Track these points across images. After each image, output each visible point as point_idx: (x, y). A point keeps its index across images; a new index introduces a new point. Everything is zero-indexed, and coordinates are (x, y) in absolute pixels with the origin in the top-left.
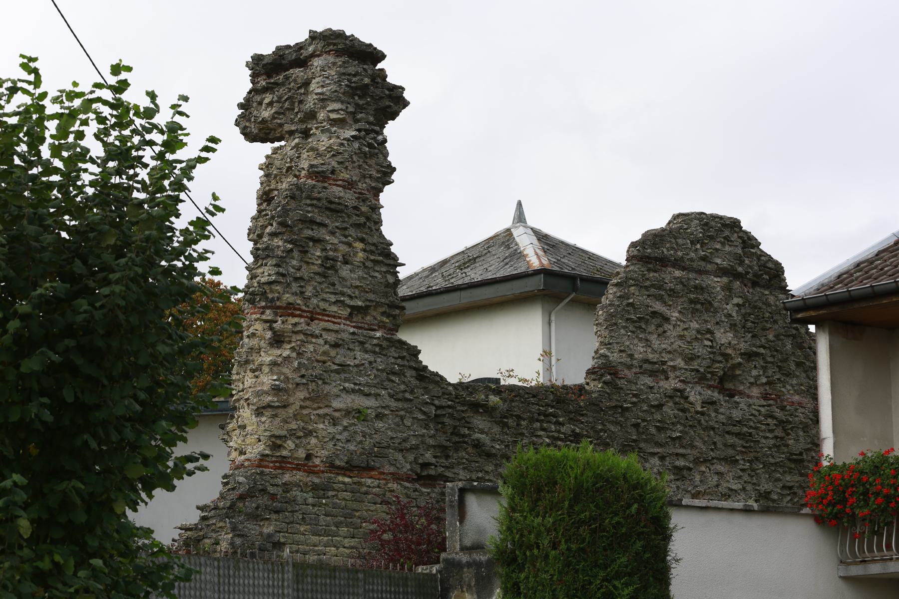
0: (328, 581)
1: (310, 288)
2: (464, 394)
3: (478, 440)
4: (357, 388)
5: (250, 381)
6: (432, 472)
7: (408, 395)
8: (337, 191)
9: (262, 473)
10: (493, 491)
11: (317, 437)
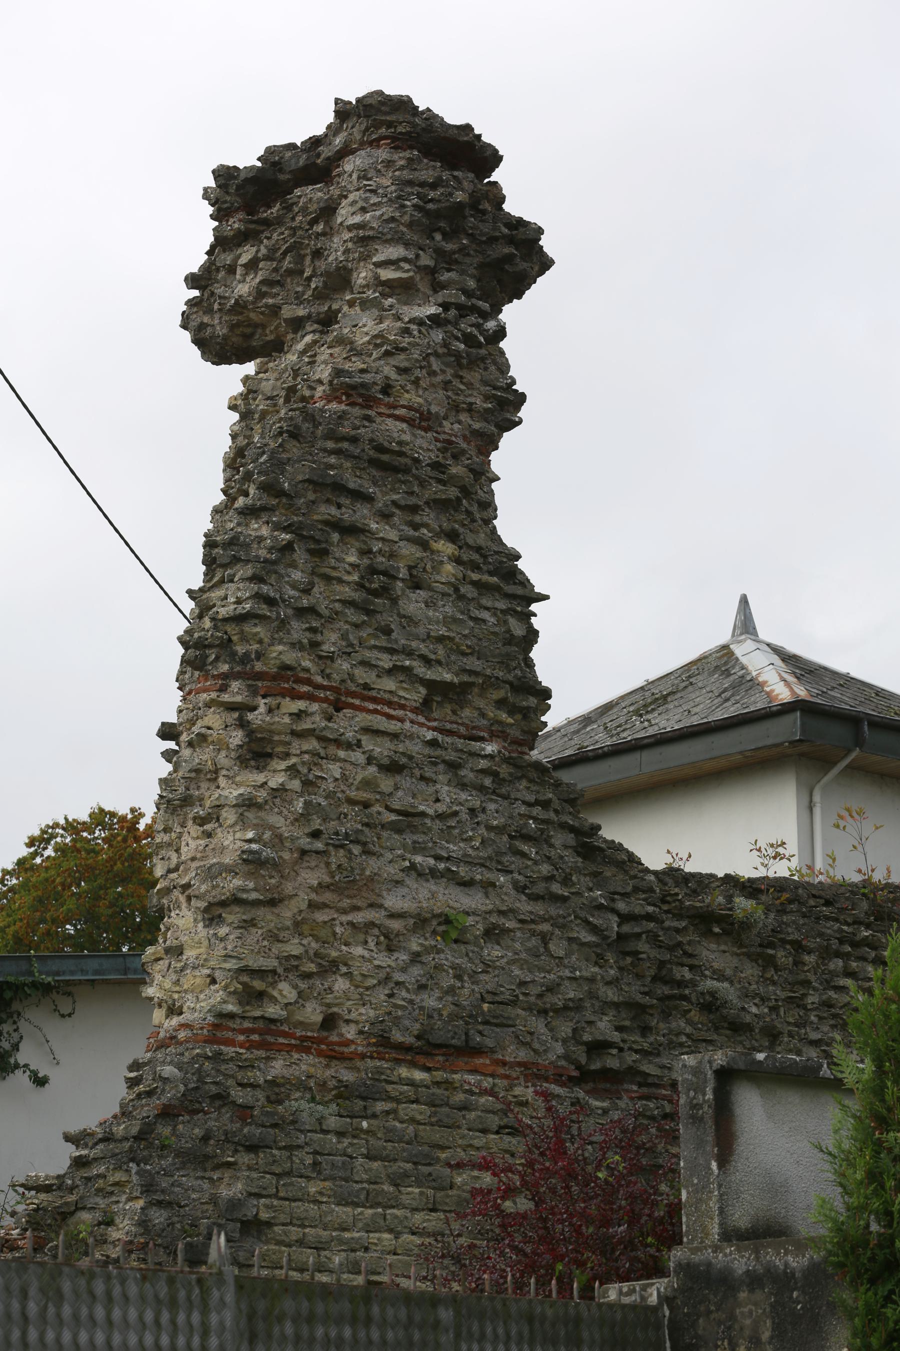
0: (347, 1332)
1: (334, 637)
2: (681, 892)
3: (712, 994)
4: (442, 866)
5: (193, 844)
6: (612, 1063)
7: (556, 888)
8: (393, 429)
9: (217, 1057)
10: (807, 1080)
11: (349, 975)
